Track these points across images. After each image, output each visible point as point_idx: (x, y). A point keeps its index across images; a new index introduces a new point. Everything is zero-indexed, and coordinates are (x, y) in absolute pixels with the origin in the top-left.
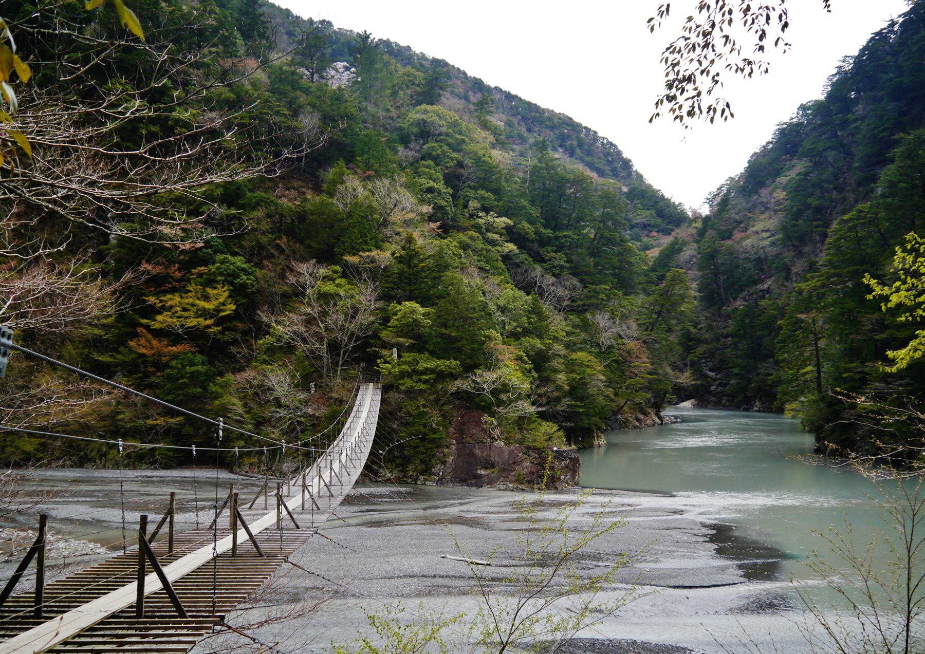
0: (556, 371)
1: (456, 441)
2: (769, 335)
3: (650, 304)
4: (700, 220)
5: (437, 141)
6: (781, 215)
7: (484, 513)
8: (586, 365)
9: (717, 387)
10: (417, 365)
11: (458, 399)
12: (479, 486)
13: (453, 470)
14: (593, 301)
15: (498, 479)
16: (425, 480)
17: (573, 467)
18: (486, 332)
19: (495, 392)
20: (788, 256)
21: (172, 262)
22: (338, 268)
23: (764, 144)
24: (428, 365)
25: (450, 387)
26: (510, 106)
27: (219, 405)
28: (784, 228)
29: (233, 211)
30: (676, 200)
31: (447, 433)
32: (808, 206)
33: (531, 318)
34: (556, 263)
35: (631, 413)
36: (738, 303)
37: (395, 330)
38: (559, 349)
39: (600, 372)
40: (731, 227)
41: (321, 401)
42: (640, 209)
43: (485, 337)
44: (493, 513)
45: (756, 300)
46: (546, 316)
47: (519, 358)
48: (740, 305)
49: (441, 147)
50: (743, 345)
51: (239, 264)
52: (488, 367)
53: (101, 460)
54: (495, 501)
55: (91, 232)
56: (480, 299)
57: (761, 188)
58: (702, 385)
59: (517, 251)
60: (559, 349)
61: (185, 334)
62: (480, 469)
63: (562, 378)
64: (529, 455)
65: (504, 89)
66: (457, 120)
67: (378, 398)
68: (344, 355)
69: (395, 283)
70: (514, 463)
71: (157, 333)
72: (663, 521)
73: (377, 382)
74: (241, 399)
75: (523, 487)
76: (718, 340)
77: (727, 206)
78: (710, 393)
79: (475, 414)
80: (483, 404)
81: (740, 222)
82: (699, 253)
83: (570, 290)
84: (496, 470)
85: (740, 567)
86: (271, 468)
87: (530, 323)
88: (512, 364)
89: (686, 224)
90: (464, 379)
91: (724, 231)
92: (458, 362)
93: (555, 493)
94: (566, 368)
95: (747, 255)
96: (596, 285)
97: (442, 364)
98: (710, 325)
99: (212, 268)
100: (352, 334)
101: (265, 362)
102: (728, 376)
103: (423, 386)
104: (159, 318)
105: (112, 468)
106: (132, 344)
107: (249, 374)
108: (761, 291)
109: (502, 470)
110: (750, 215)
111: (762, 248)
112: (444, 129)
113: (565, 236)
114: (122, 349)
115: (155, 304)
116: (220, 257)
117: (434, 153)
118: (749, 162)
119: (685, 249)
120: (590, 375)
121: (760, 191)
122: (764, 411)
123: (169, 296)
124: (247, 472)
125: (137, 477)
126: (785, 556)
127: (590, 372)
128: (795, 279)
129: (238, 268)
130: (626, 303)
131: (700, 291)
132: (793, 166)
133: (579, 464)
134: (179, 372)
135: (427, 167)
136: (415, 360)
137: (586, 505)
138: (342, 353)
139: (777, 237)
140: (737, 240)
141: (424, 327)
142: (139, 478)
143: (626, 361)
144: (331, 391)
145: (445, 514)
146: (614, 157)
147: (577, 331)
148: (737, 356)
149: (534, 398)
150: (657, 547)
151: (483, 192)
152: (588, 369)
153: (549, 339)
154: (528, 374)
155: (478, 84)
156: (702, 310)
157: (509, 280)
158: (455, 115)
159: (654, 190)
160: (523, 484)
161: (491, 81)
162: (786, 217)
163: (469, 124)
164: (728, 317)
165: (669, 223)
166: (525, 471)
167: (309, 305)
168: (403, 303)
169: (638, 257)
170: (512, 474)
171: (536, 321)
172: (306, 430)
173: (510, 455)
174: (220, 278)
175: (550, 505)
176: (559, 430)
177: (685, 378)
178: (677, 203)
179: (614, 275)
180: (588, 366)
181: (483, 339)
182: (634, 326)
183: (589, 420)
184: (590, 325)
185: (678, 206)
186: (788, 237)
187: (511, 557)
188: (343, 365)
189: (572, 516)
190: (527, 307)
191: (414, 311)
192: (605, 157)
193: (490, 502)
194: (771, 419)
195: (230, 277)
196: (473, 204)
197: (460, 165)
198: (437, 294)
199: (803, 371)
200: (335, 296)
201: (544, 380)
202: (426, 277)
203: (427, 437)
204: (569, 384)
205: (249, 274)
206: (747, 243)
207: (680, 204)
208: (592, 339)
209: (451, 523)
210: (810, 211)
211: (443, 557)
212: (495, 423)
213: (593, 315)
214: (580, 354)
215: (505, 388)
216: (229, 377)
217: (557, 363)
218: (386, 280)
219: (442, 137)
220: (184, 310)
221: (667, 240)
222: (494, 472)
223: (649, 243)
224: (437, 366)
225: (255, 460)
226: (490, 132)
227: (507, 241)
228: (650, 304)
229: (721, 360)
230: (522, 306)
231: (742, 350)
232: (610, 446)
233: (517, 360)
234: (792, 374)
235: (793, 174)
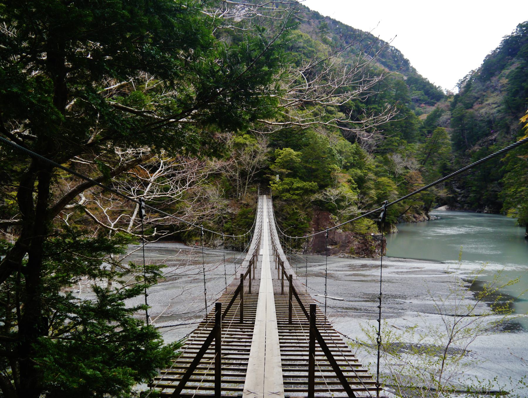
0: (370, 189)
2: (495, 167)
3: (423, 148)
4: (452, 97)
5: (297, 51)
6: (504, 93)
7: (334, 271)
10: (292, 185)
12: (328, 255)
13: (313, 245)
14: (390, 147)
15: (339, 251)
17: (383, 245)
18: (331, 166)
19: (337, 201)
20: (508, 119)
23: (495, 49)
24: (299, 185)
25: (312, 198)
26: (335, 28)
28: (506, 102)
30: (437, 84)
31: (310, 224)
32: (522, 88)
33: (355, 157)
35: (411, 214)
36: (476, 148)
37: (279, 165)
38: (371, 175)
39: (395, 189)
40: (472, 101)
41: (236, 205)
42: (414, 90)
43: (331, 168)
44: (339, 271)
45: (487, 146)
46: (364, 156)
47: (349, 181)
48: (477, 149)
49: (300, 55)
50: (479, 173)
52: (333, 186)
54: (338, 264)
56: (328, 146)
57: (492, 77)
58: (453, 197)
60: (371, 175)
62: (329, 245)
63: (373, 192)
64: (357, 238)
65: (332, 17)
66: (309, 39)
67: (271, 204)
68: (249, 179)
69: (278, 137)
70: (348, 242)
72: (439, 277)
75: (354, 256)
77: (470, 88)
78: (457, 202)
80: (330, 208)
81: (478, 98)
82: (452, 117)
84: (338, 246)
85: (489, 305)
87: (354, 160)
88: (346, 185)
89: (443, 100)
91: (468, 103)
92: (316, 183)
94: (375, 187)
95: (482, 118)
97: (307, 184)
98: (458, 161)
100: (254, 167)
102: (468, 191)
103: (297, 197)
108: (491, 140)
109: (342, 246)
110: (485, 94)
111: (492, 114)
112: (302, 44)
113: (374, 108)
118: (484, 61)
119: (443, 114)
120: (390, 191)
121: (491, 79)
122: (490, 213)
126: (517, 300)
128: (512, 133)
130: (409, 148)
131: (452, 140)
132: (513, 63)
133: (386, 244)
136: (291, 182)
137: (392, 267)
138: (248, 178)
139: (501, 107)
140: (476, 109)
141: (295, 163)
143: (409, 183)
145: (312, 271)
146: (398, 58)
147: (381, 165)
148: (474, 180)
149: (362, 205)
150: (438, 292)
153: (366, 170)
154: (355, 190)
155: (316, 15)
156: (453, 152)
158: (308, 35)
159: (423, 79)
161: (324, 13)
162: (507, 95)
163: (315, 40)
164: (470, 156)
165: (432, 99)
166: (355, 247)
169: (416, 120)
171: (358, 159)
172: (228, 222)
173: (346, 237)
175: (371, 267)
176: (373, 224)
177: (443, 193)
178: (437, 87)
179: (402, 131)
180: (388, 186)
181: (330, 170)
182: (416, 163)
184: (389, 162)
185: (438, 88)
186: (509, 108)
187: (354, 296)
188: (248, 185)
189: (386, 273)
190: (353, 151)
191: (290, 154)
192: (393, 58)
193: (335, 265)
194: (497, 218)
198: (303, 144)
199: (519, 190)
201: (364, 194)
202: (297, 133)
204: (377, 196)
206: (483, 111)
207: (439, 87)
208: (391, 169)
209: (316, 276)
210: (524, 91)
212: (337, 219)
214: (383, 178)
215: (343, 198)
217: (371, 184)
219: (300, 49)
221: (431, 109)
222: (336, 247)
223: (420, 111)
224: (304, 186)
225: (199, 238)
226: (328, 45)
227: (339, 111)
228: (423, 148)
229: (464, 182)
231: (478, 176)
232: (400, 232)
234: (513, 191)
235: (513, 68)
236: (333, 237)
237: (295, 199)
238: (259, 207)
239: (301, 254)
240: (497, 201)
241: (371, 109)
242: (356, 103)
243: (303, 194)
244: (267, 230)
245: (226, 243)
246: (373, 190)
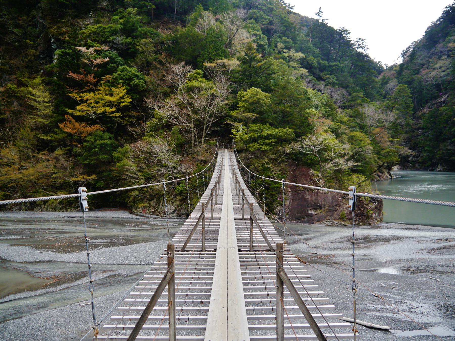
1: (291, 189)
9: (413, 158)
10: (262, 132)
12: (311, 222)
13: (290, 210)
15: (325, 218)
19: (319, 152)
21: (88, 72)
22: (200, 71)
27: (119, 166)
29: (129, 40)
34: (330, 81)
36: (425, 110)
41: (191, 162)
48: (426, 111)
51: (133, 72)
53: (45, 205)
55: (42, 60)
57: (436, 44)
59: (308, 74)
61: (97, 118)
62: (311, 210)
71: (79, 119)
74: (134, 162)
76: (413, 131)
78: (408, 161)
80: (309, 161)
81: (424, 65)
86: (157, 210)
97: (281, 131)
99: (115, 75)
101: (151, 136)
104: (79, 108)
105: (52, 211)
106: (61, 126)
107: (140, 144)
108: (439, 102)
109: (329, 211)
113: (335, 65)
114: (56, 130)
115: (76, 98)
116: (120, 68)
117: (255, 16)
118: (425, 32)
122: (444, 171)
123: (86, 94)
124: (141, 213)
125: (64, 217)
129: (133, 74)
134: (92, 144)
135: (251, 24)
138: (204, 128)
142: (65, 218)
151: (286, 38)
153: (338, 122)
160: (345, 221)
164: (419, 118)
168: (248, 90)
170: (336, 213)
171: (329, 111)
174: (121, 81)
178: (377, 62)
188: (205, 137)
195: (127, 81)
196: (280, 45)
197: (271, 23)
200: (200, 89)
205: (141, 79)
207: (379, 62)
212: (320, 175)
215: (326, 149)
216: (127, 147)
220: (97, 103)
222: (321, 212)
227: (301, 67)
229: (415, 143)
236: (315, 199)
237: (266, 151)
239: (275, 223)
240: (451, 159)
241: (333, 66)
242: (318, 60)
243: (276, 143)
244: (230, 192)
245: (179, 210)
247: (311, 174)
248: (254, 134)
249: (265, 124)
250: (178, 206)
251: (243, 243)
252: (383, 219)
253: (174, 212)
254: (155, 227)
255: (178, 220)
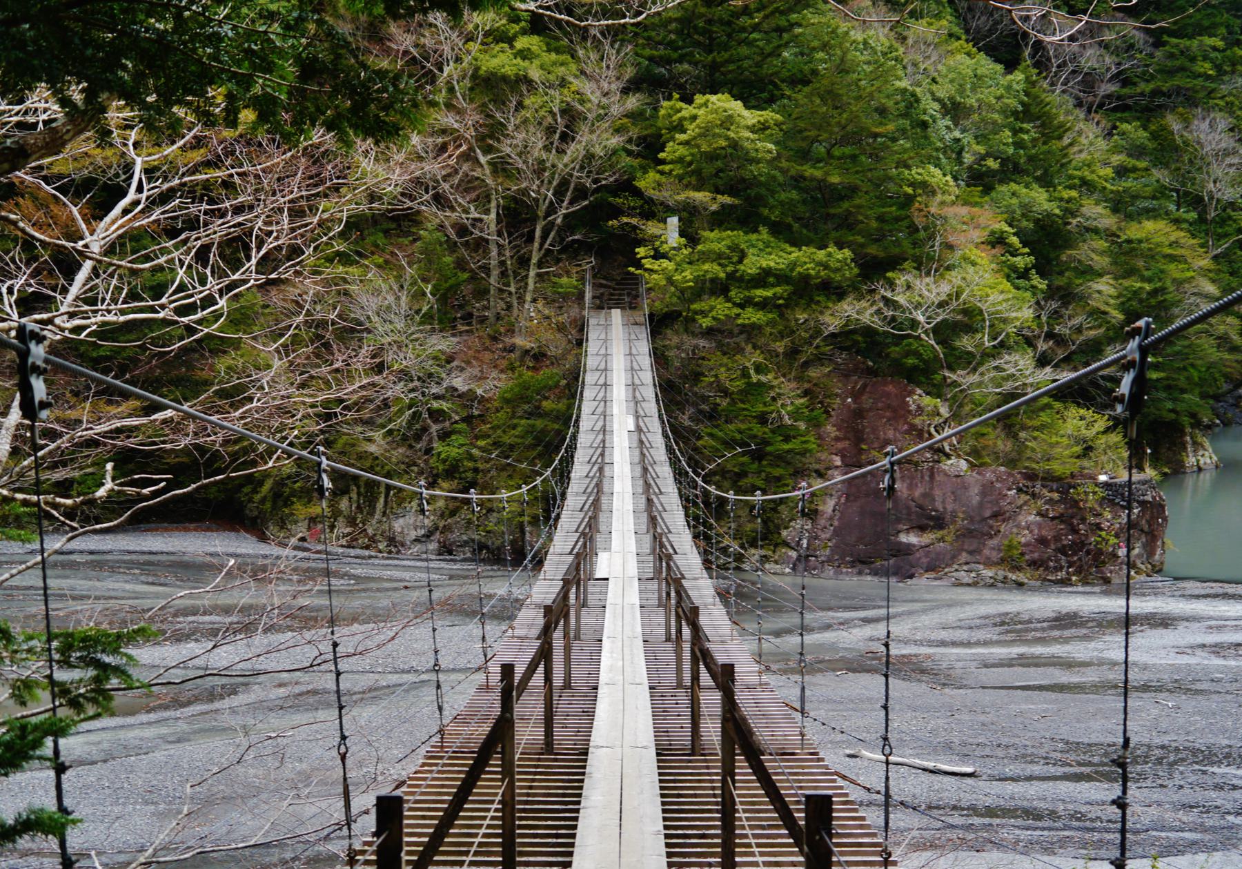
0: (1089, 272)
1: (843, 457)
7: (931, 643)
8: (1166, 256)
10: (740, 261)
11: (842, 349)
13: (836, 533)
14: (1179, 81)
15: (954, 558)
16: (765, 559)
18: (916, 173)
19: (944, 332)
31: (820, 437)
33: (1021, 130)
37: (678, 170)
38: (1096, 212)
39: (1205, 272)
41: (487, 356)
43: (912, 184)
44: (954, 644)
46: (1061, 125)
47: (997, 241)
52: (923, 265)
54: (951, 616)
56: (898, 84)
60: (1096, 212)
63: (1104, 290)
64: (1034, 496)
67: (643, 347)
68: (544, 238)
69: (671, 45)
70: (995, 516)
73: (633, 307)
75: (1021, 577)
79: (890, 388)
80: (911, 361)
83: (1116, 52)
84: (949, 534)
87: (1019, 145)
88: (983, 257)
90: (860, 297)
92: (847, 253)
93: (1105, 593)
94: (1115, 263)
96: (1191, 37)
100: (564, 183)
109: (966, 534)
120: (1179, 283)
127: (1177, 275)
133: (1165, 519)
136: (734, 248)
138: (538, 233)
141: (758, 161)
144: (511, 331)
145: (833, 647)
147: (1142, 164)
152: (1172, 267)
153: (1071, 187)
154: (1021, 282)
157: (956, 29)
160: (1019, 569)
166: (1025, 537)
167: (449, 106)
170: (993, 543)
171: (1034, 140)
175: (1100, 625)
176: (1107, 431)
180: (1172, 258)
181: (910, 190)
183: (1175, 400)
184: (1176, 149)
188: (540, 264)
190: (1012, 102)
191: (728, 121)
198: (785, 74)
202: (756, 28)
203: (769, 449)
204: (1122, 307)
208: (1184, 185)
209: (854, 671)
211: (850, 756)
212: (944, 411)
213: (1187, 123)
214: (1149, 225)
217: (1093, 252)
218: (649, 39)
222: (942, 539)
224: (793, 265)
230: (999, 98)
233: (993, 245)
236: (924, 495)
237: (754, 326)
238: (591, 362)
239: (783, 574)
245: (447, 529)
246: (1106, 278)
247: (913, 407)
248: (716, 267)
249: (756, 231)
250: (442, 516)
251: (691, 774)
252: (1165, 568)
253: (428, 536)
254: (374, 585)
255: (443, 565)
